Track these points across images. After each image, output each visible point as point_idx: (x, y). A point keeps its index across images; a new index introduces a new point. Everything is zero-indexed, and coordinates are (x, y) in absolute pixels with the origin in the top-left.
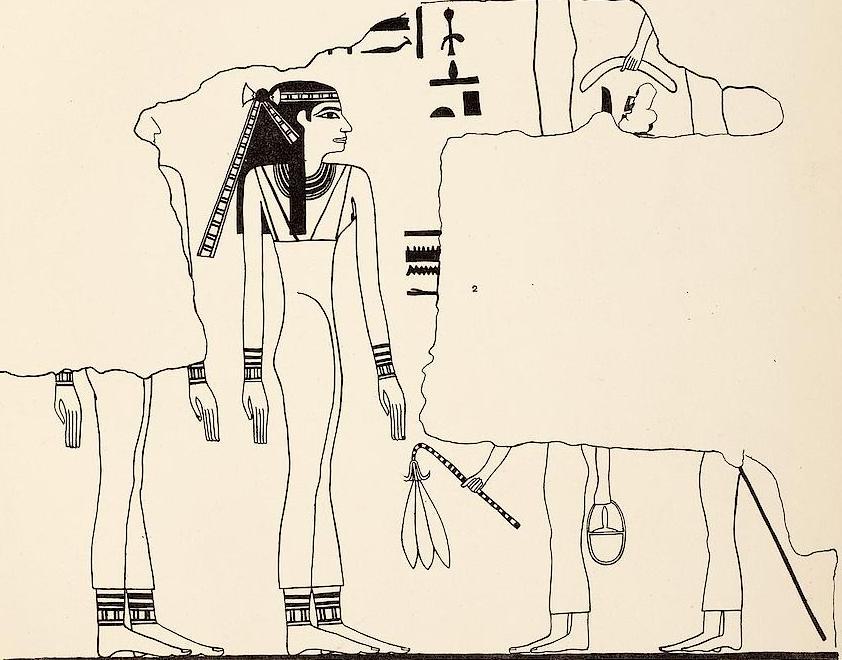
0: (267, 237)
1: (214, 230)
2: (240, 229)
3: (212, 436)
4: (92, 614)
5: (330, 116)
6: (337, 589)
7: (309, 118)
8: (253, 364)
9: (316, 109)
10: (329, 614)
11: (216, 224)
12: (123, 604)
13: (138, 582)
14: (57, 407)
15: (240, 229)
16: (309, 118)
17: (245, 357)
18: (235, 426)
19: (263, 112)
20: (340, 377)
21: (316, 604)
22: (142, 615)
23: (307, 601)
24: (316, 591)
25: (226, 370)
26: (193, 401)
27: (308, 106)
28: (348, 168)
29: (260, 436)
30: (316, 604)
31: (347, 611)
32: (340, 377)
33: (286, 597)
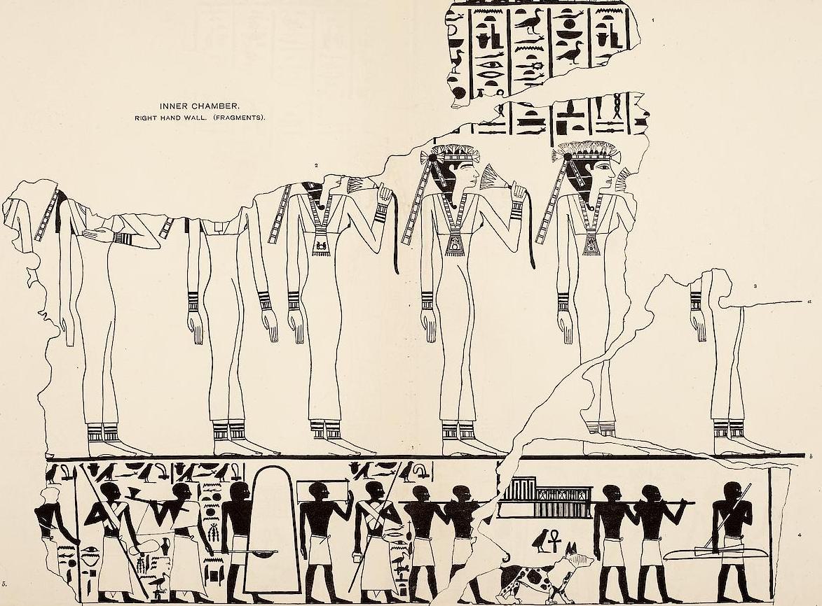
0: (202, 233)
1: (275, 232)
2: (58, 230)
3: (274, 339)
4: (211, 434)
5: (604, 168)
6: (742, 421)
7: (592, 168)
8: (294, 299)
9: (597, 164)
10: (738, 433)
11: (44, 225)
12: (727, 427)
13: (736, 415)
14: (290, 322)
15: (58, 230)
16: (592, 168)
17: (423, 297)
18: (286, 334)
19: (568, 165)
20: (242, 312)
21: (327, 428)
22: (721, 433)
23: (322, 426)
24: (731, 421)
25: (280, 301)
26: (559, 321)
27: (592, 163)
28: (344, 197)
29: (702, 339)
30: (327, 428)
31: (121, 434)
32: (242, 312)
33: (214, 425)
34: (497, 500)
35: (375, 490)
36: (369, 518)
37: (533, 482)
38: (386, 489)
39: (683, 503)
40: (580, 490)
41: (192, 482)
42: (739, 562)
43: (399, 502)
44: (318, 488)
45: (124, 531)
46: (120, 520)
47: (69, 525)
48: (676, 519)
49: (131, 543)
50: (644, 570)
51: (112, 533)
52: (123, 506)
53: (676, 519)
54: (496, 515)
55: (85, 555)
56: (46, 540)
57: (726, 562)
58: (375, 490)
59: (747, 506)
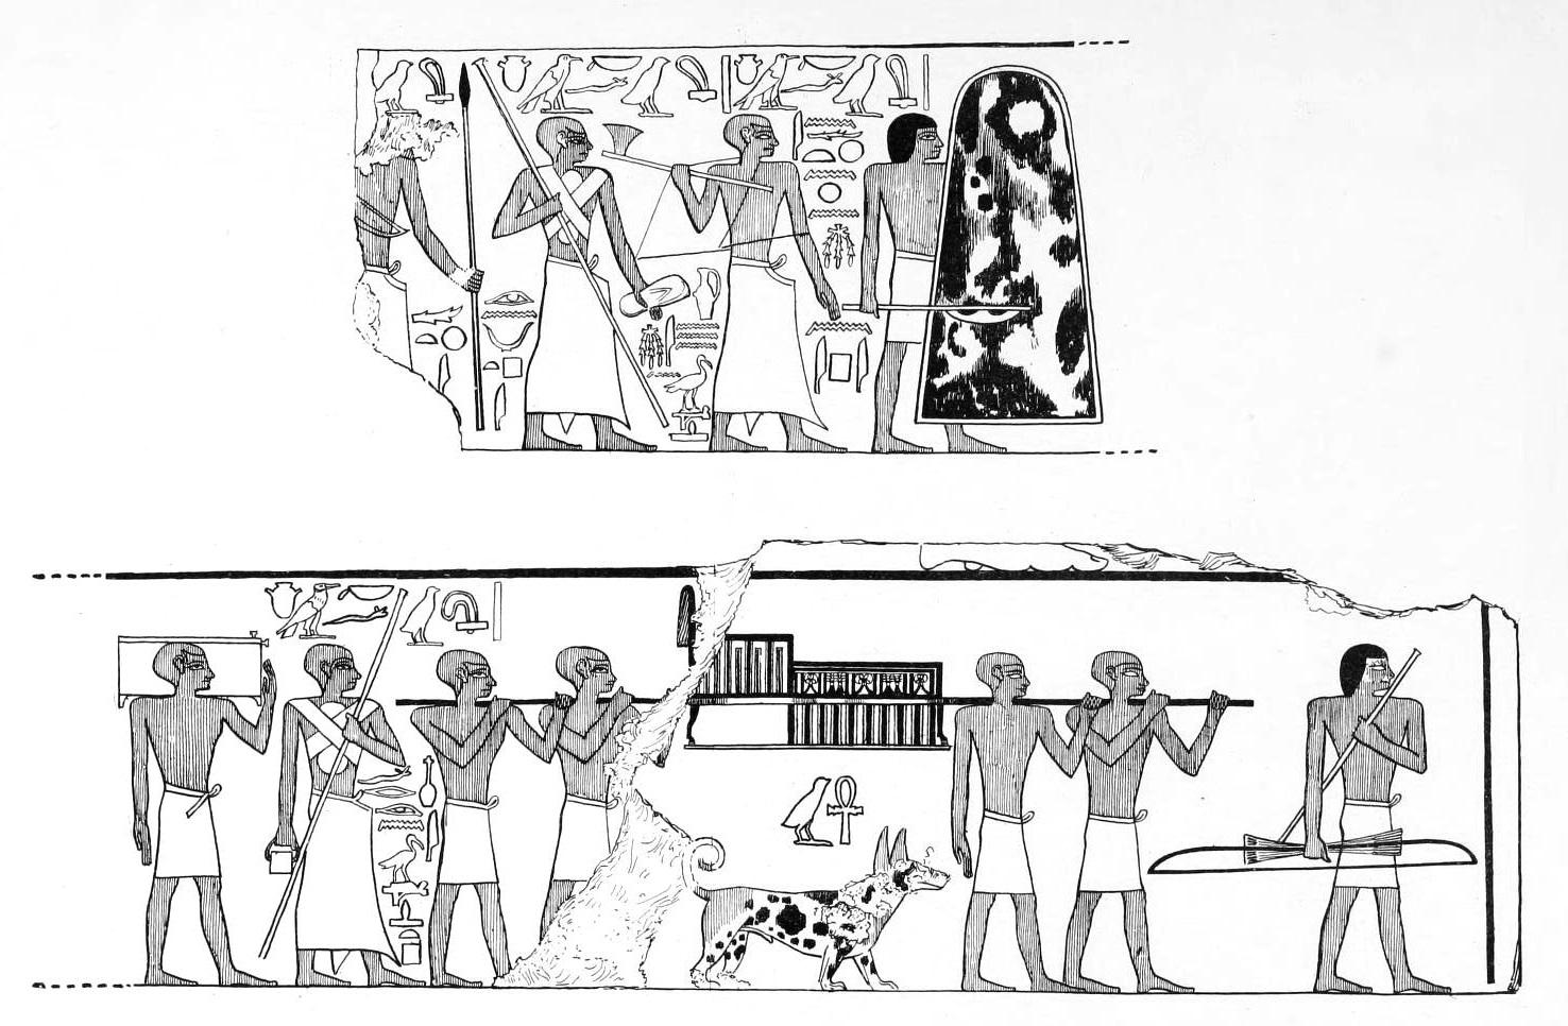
34: (688, 688)
35: (334, 668)
36: (316, 743)
37: (784, 645)
38: (362, 664)
39: (1217, 704)
40: (921, 667)
41: (580, 233)
42: (1385, 878)
43: (400, 703)
44: (188, 659)
45: (599, 244)
46: (588, 217)
47: (448, 225)
48: (1188, 761)
49: (620, 286)
50: (1086, 901)
51: (576, 253)
52: (598, 178)
53: (1188, 761)
54: (681, 738)
55: (494, 315)
56: (376, 279)
57: (1346, 878)
58: (334, 668)
59: (1415, 725)
